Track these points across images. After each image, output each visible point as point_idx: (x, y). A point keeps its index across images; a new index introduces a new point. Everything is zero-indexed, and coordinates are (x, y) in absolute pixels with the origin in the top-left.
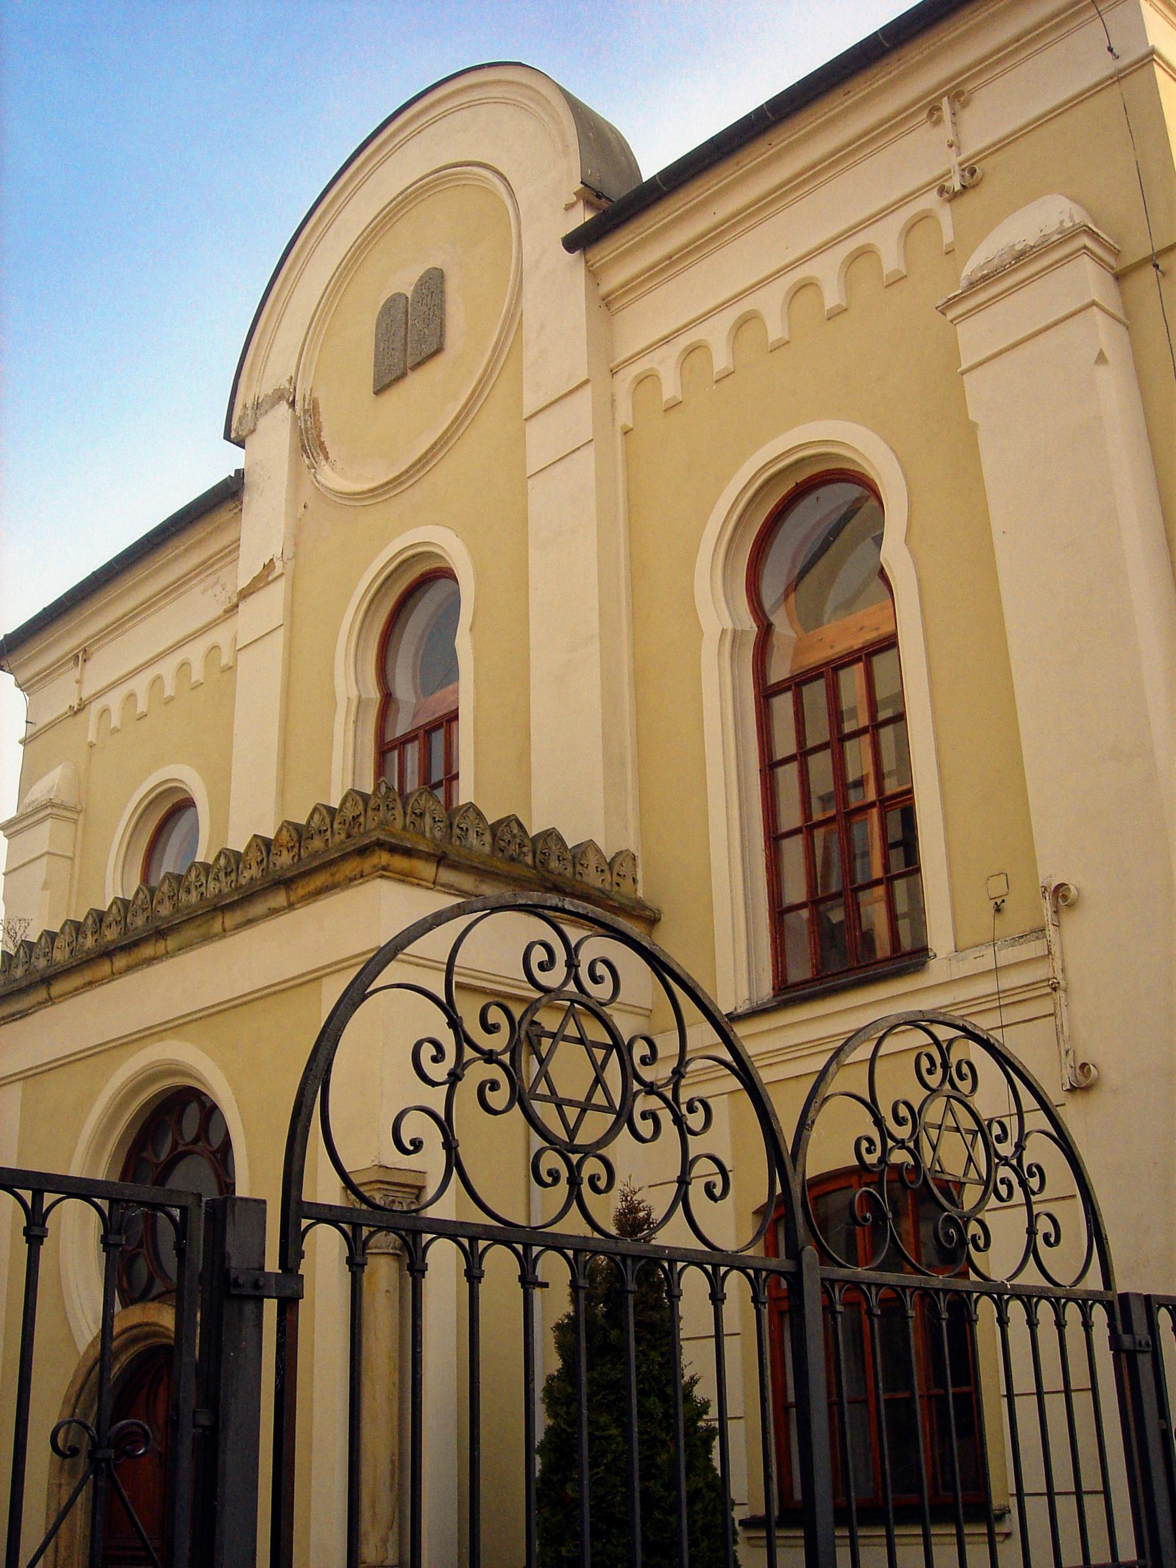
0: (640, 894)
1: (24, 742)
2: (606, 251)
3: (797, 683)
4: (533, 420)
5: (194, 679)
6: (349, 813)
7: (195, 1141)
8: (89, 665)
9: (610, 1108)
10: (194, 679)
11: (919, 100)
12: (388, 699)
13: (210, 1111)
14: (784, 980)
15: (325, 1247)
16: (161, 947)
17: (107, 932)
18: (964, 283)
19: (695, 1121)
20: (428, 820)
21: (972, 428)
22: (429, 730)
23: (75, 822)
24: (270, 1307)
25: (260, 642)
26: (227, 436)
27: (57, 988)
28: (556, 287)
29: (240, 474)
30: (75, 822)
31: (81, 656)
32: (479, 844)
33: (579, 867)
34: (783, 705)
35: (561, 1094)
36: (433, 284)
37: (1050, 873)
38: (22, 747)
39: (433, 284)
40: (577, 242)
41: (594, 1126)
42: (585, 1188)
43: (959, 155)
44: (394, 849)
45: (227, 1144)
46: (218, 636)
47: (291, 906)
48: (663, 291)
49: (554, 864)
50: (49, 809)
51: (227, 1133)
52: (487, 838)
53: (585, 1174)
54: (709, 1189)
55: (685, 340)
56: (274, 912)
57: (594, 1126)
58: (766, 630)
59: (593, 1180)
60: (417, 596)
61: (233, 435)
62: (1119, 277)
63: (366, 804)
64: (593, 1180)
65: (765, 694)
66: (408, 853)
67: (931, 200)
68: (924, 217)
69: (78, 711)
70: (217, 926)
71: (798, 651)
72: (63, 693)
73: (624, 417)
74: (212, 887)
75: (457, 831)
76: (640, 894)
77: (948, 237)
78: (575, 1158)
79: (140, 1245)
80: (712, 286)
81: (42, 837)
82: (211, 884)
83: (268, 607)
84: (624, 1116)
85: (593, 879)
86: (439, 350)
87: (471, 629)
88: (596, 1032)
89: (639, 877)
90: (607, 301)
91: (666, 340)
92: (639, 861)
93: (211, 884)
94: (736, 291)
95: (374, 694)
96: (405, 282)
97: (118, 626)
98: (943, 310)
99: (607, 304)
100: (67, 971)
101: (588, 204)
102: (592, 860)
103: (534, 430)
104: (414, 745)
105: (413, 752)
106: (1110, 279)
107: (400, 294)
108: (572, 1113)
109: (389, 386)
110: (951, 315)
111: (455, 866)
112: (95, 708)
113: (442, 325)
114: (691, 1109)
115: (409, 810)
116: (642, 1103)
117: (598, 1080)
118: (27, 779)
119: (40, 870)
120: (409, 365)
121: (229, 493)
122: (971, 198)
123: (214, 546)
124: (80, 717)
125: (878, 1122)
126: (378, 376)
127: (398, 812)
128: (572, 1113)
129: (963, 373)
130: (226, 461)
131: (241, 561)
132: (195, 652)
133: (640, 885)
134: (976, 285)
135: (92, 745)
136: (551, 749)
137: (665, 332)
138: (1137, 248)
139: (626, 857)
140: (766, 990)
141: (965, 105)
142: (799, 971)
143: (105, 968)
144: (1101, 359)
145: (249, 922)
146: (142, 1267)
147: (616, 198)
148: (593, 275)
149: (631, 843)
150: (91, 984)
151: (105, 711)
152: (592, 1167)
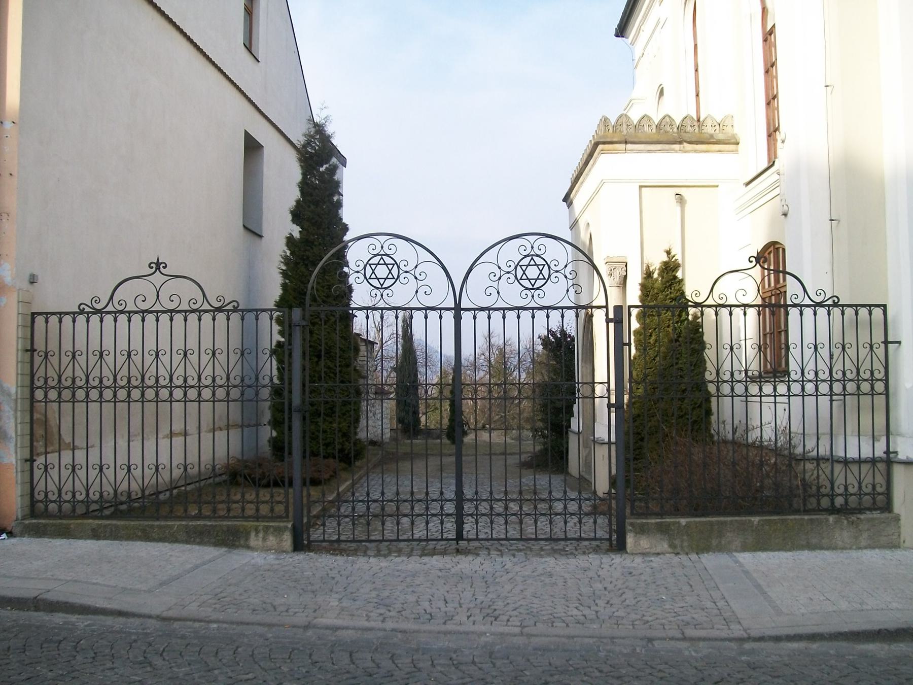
20: (624, 126)
49: (689, 129)
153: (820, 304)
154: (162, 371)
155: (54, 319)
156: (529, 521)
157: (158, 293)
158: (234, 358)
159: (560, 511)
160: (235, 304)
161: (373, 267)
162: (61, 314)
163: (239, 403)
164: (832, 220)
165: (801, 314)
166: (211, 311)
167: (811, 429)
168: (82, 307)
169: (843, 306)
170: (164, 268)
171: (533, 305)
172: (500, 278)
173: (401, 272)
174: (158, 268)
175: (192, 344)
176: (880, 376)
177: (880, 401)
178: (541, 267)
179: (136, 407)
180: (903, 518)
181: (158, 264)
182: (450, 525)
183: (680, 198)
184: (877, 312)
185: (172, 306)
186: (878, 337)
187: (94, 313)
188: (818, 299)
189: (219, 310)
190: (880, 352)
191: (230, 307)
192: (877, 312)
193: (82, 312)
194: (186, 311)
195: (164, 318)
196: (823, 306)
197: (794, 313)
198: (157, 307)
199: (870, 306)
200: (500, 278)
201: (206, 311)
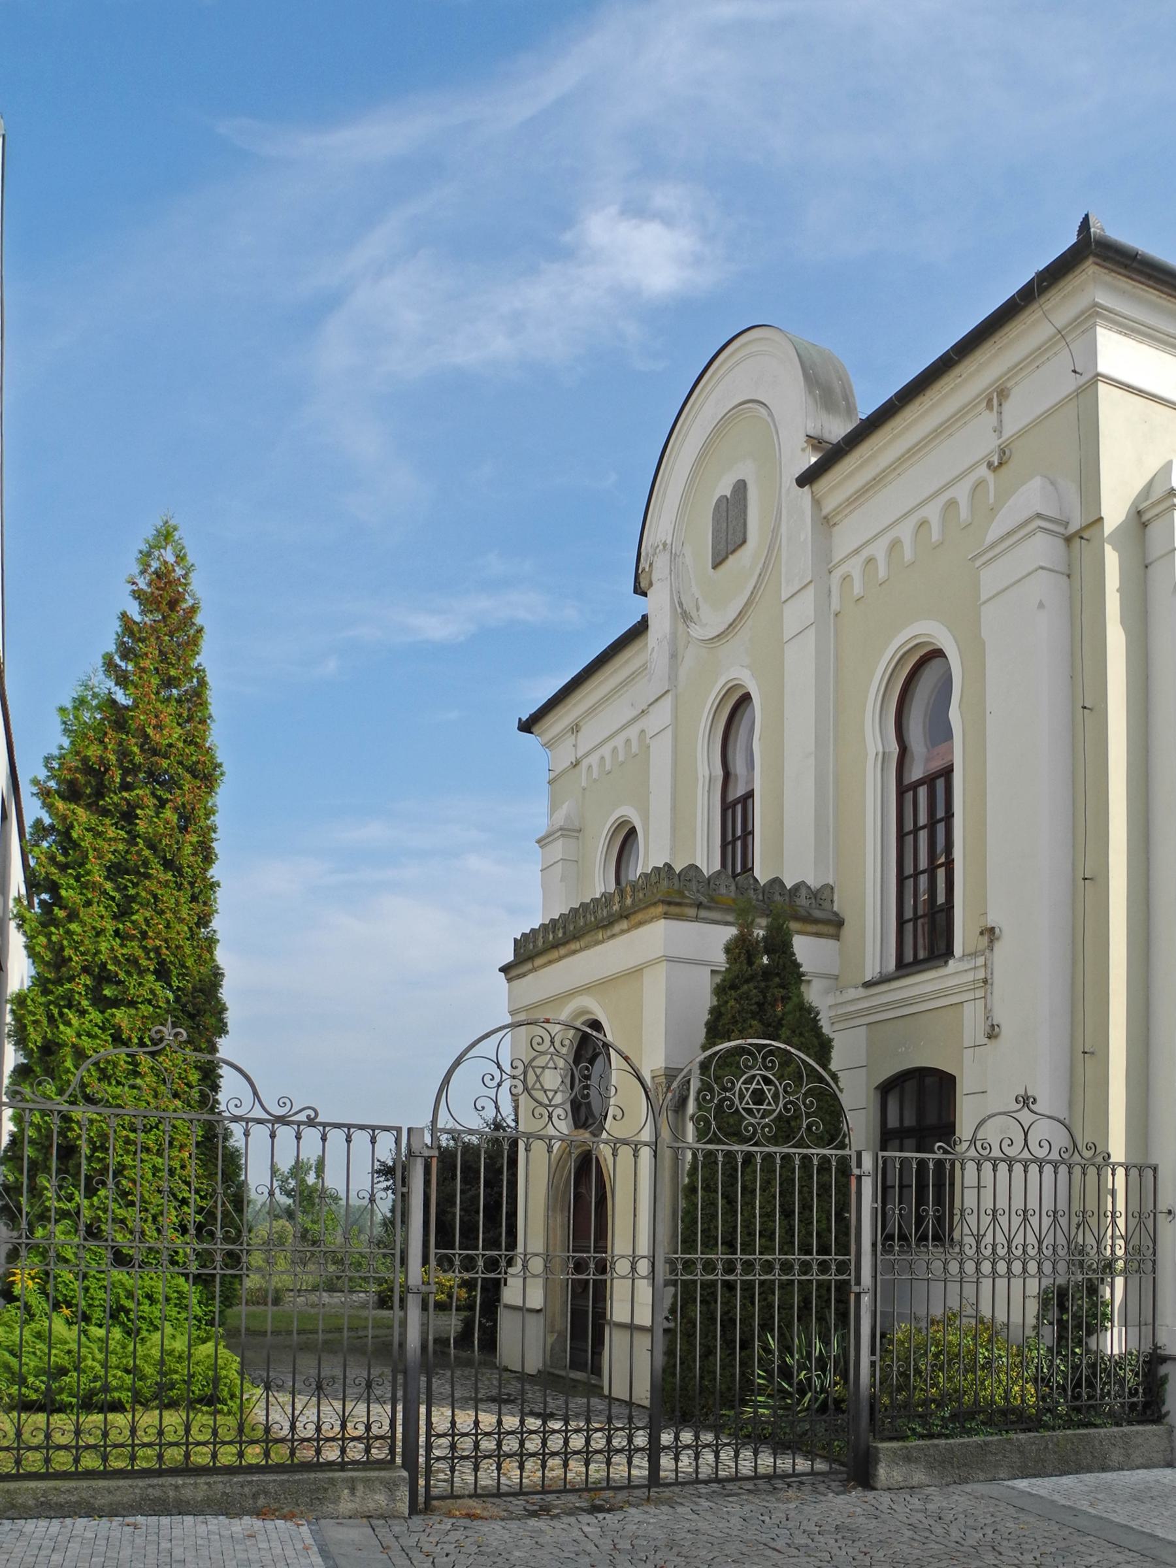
0: (835, 909)
2: (824, 483)
5: (633, 750)
11: (979, 395)
22: (929, 781)
31: (575, 729)
36: (741, 487)
40: (807, 479)
49: (777, 898)
55: (865, 553)
56: (623, 932)
62: (1068, 540)
65: (902, 790)
66: (679, 904)
67: (983, 471)
68: (980, 484)
69: (576, 765)
71: (928, 760)
73: (835, 605)
76: (835, 909)
77: (991, 500)
78: (550, 1109)
81: (558, 849)
83: (662, 715)
86: (744, 542)
89: (835, 898)
91: (856, 551)
92: (836, 890)
94: (875, 533)
95: (719, 772)
96: (725, 488)
97: (591, 711)
99: (826, 523)
100: (540, 954)
101: (815, 448)
102: (803, 892)
103: (788, 610)
105: (923, 791)
106: (1060, 543)
108: (550, 1094)
109: (720, 563)
110: (978, 563)
111: (708, 908)
112: (584, 764)
119: (558, 868)
121: (641, 628)
122: (1004, 468)
128: (550, 1094)
133: (836, 905)
137: (855, 546)
143: (554, 954)
144: (1041, 605)
145: (613, 936)
147: (835, 441)
150: (550, 962)
153: (282, 1120)
154: (1001, 1239)
156: (619, 1459)
157: (496, 1103)
159: (377, 1444)
160: (313, 1115)
161: (538, 1071)
165: (348, 1140)
166: (268, 1121)
167: (1016, 1318)
169: (324, 1125)
172: (499, 1085)
173: (522, 1077)
175: (1033, 1204)
178: (538, 1071)
180: (847, 1504)
182: (641, 1463)
185: (1041, 1153)
188: (280, 1112)
189: (282, 1120)
191: (302, 1117)
196: (288, 1123)
198: (1026, 1155)
199: (349, 1126)
200: (499, 1085)
201: (260, 1121)
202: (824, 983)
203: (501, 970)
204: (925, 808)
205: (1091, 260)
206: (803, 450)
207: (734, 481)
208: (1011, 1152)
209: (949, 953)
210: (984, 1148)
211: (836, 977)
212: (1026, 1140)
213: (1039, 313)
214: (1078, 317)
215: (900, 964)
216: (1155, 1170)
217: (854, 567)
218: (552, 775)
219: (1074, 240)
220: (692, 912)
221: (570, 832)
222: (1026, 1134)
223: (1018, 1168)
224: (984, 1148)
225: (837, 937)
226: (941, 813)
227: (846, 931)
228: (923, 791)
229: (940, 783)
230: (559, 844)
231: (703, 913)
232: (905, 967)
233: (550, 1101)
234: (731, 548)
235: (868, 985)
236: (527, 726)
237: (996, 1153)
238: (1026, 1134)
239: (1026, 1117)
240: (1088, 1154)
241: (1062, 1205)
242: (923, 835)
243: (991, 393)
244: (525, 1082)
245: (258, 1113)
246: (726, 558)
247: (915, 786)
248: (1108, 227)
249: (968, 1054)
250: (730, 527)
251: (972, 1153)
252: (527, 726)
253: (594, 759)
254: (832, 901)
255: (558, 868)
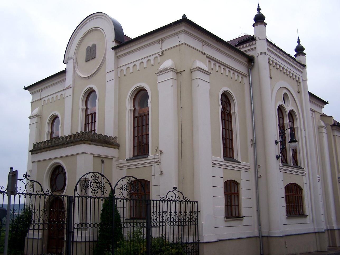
0: (118, 142)
1: (31, 103)
2: (118, 50)
3: (138, 117)
4: (107, 73)
6: (80, 134)
7: (61, 172)
8: (42, 92)
9: (98, 187)
10: (59, 99)
12: (87, 109)
13: (63, 168)
14: (134, 155)
15: (77, 198)
16: (56, 147)
17: (49, 144)
18: (159, 71)
19: (105, 188)
20: (90, 136)
21: (158, 91)
22: (92, 114)
23: (40, 117)
24: (73, 202)
25: (70, 96)
26: (64, 63)
27: (42, 150)
28: (111, 54)
29: (66, 69)
30: (40, 117)
31: (41, 91)
32: (97, 138)
33: (110, 140)
34: (136, 119)
35: (94, 187)
36: (94, 46)
37: (160, 149)
38: (31, 103)
39: (94, 46)
41: (96, 189)
42: (95, 193)
43: (161, 50)
44: (86, 140)
45: (65, 173)
46: (63, 93)
47: (73, 145)
48: (125, 57)
49: (106, 139)
50: (37, 116)
51: (65, 172)
52: (98, 137)
53: (95, 192)
54: (106, 193)
57: (96, 189)
58: (135, 109)
59: (96, 193)
60: (90, 93)
61: (65, 63)
62: (177, 73)
63: (83, 133)
64: (96, 193)
67: (157, 55)
68: (156, 57)
70: (64, 146)
71: (139, 111)
72: (38, 96)
73: (119, 75)
74: (63, 141)
75: (94, 137)
76: (118, 142)
79: (54, 184)
80: (132, 58)
81: (35, 120)
82: (63, 140)
83: (69, 92)
84: (99, 188)
85: (111, 141)
86: (95, 58)
87: (98, 102)
88: (97, 181)
89: (118, 140)
90: (118, 57)
92: (118, 138)
93: (63, 140)
95: (85, 107)
98: (157, 74)
99: (117, 58)
104: (90, 118)
105: (90, 116)
106: (175, 73)
107: (90, 46)
108: (95, 188)
111: (93, 142)
112: (43, 100)
113: (95, 53)
114: (105, 187)
115: (89, 135)
116: (100, 187)
117: (97, 185)
118: (32, 109)
120: (91, 59)
121: (64, 72)
122: (162, 57)
123: (62, 79)
124: (41, 101)
125: (122, 186)
126: (86, 59)
127: (87, 135)
129: (158, 83)
130: (63, 67)
131: (66, 81)
132: (59, 94)
134: (161, 71)
135: (43, 106)
136: (107, 125)
138: (179, 71)
139: (116, 137)
140: (132, 156)
141: (163, 42)
142: (136, 154)
144: (172, 86)
146: (54, 187)
148: (116, 53)
149: (117, 135)
151: (45, 100)
152: (96, 192)
154: (161, 218)
155: (155, 202)
157: (26, 186)
158: (41, 213)
162: (156, 201)
163: (43, 230)
164: (182, 178)
168: (161, 198)
169: (190, 201)
170: (28, 177)
171: (95, 196)
173: (100, 185)
174: (175, 189)
176: (196, 220)
177: (197, 226)
179: (169, 227)
181: (26, 175)
183: (103, 161)
184: (196, 203)
186: (196, 210)
187: (96, 198)
188: (46, 193)
190: (196, 214)
192: (196, 203)
193: (161, 200)
194: (35, 194)
195: (97, 199)
197: (152, 202)
198: (175, 200)
202: (116, 159)
203: (30, 151)
204: (141, 122)
205: (184, 22)
206: (113, 42)
207: (295, 51)
208: (173, 199)
209: (147, 153)
210: (168, 198)
211: (118, 158)
212: (26, 188)
213: (172, 28)
214: (180, 31)
215: (134, 156)
216: (197, 202)
217: (124, 68)
218: (33, 101)
219: (181, 18)
220: (90, 142)
221: (39, 116)
222: (175, 195)
223: (174, 202)
224: (168, 198)
225: (118, 149)
226: (93, 121)
227: (121, 147)
228: (90, 116)
229: (94, 115)
230: (36, 119)
231: (92, 143)
232: (135, 157)
233: (95, 189)
234: (91, 58)
235: (127, 160)
236: (26, 88)
237: (170, 200)
238: (175, 195)
239: (175, 192)
240: (186, 199)
241: (177, 210)
242: (90, 124)
243: (160, 41)
244: (126, 189)
245: (42, 193)
246: (90, 60)
247: (89, 115)
248: (189, 17)
249: (153, 177)
250: (91, 54)
251: (166, 199)
252: (26, 88)
253: (46, 99)
254: (117, 140)
255: (35, 125)
